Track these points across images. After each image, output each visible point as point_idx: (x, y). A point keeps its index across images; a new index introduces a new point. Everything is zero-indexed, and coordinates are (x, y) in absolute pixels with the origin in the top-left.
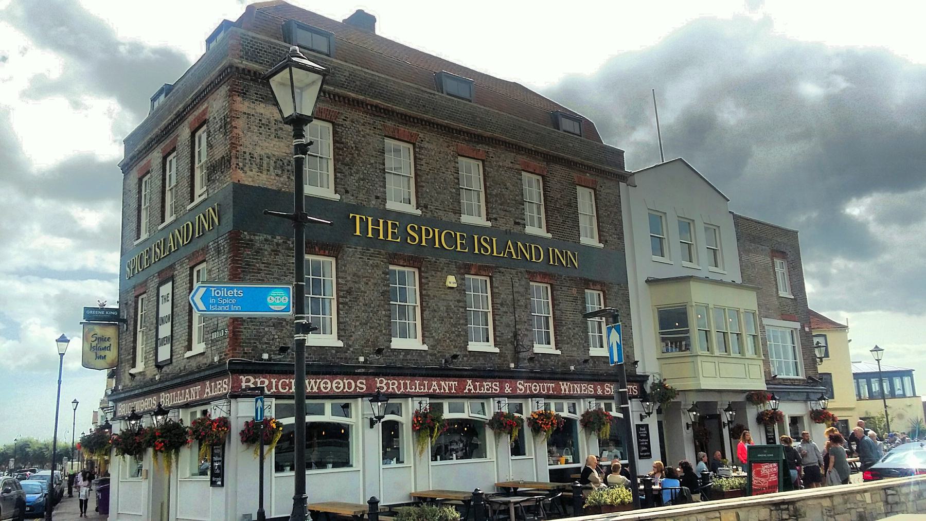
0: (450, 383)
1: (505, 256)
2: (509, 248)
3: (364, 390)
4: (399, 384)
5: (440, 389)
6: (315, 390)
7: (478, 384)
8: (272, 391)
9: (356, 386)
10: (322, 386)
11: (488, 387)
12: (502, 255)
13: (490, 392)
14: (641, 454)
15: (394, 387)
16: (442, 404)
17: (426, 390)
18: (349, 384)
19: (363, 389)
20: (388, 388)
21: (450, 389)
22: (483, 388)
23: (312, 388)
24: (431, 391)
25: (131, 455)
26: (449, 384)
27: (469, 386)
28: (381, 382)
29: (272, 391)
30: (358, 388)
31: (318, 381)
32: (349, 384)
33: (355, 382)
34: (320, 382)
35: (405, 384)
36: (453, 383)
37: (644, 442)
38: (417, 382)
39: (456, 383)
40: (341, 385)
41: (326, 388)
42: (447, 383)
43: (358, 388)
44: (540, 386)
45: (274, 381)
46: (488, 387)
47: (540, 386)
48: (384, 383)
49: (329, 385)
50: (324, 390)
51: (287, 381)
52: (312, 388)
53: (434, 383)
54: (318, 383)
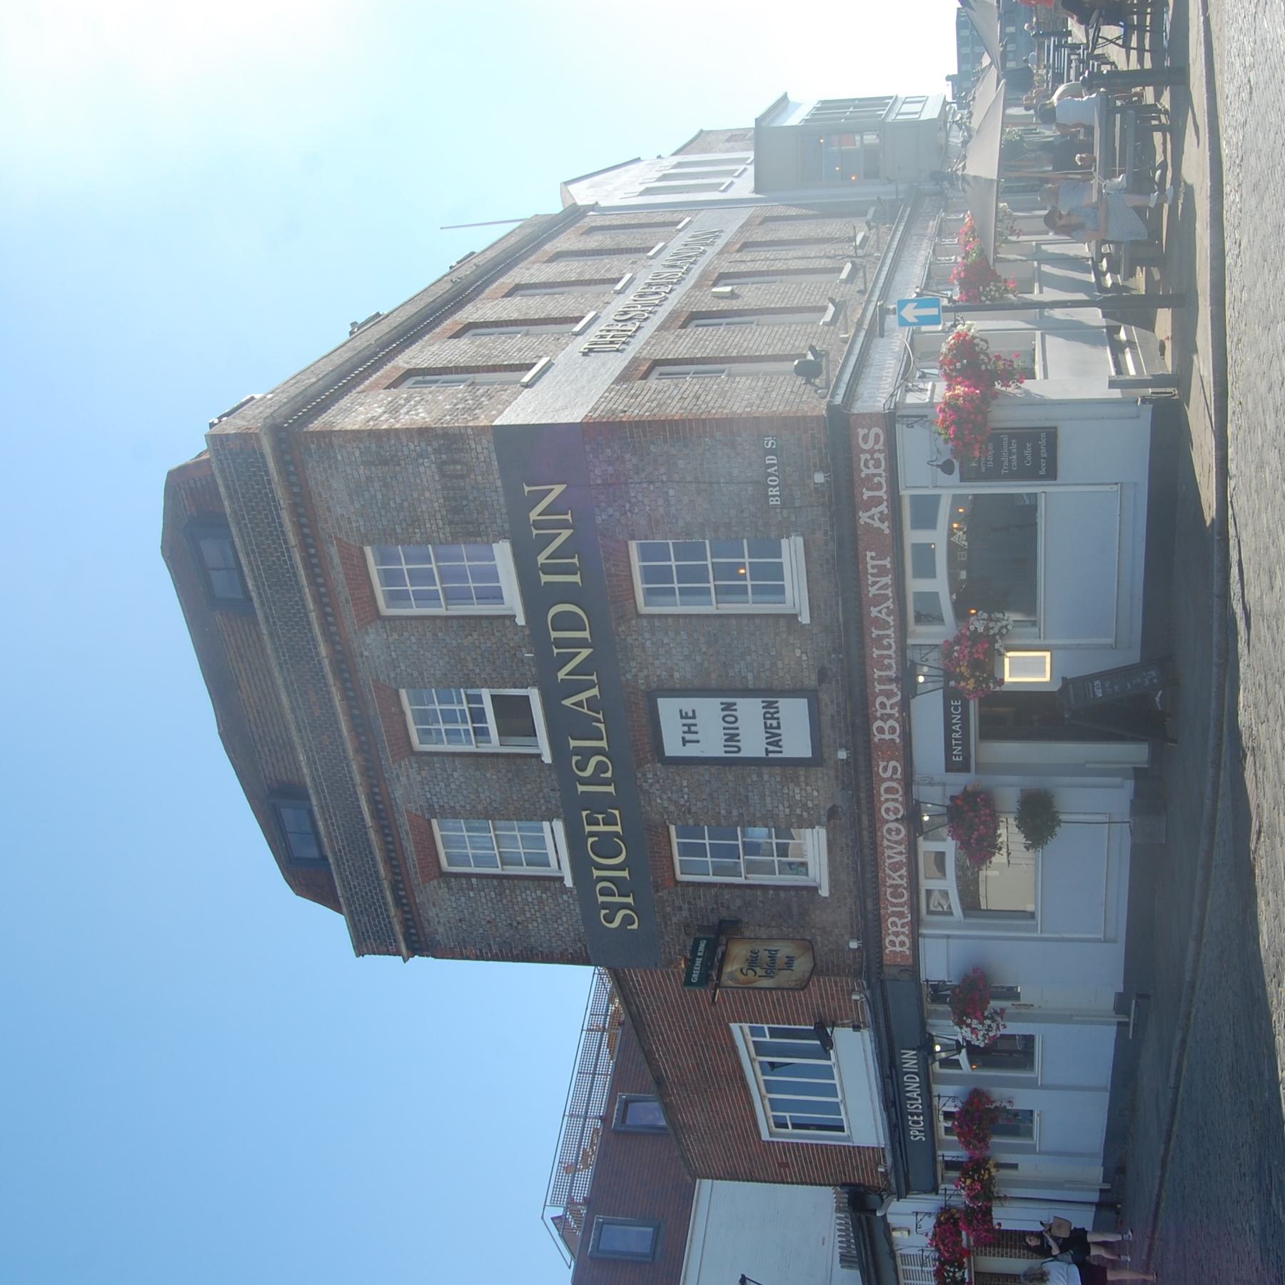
0: (871, 571)
1: (594, 677)
2: (579, 704)
3: (897, 764)
4: (894, 914)
5: (886, 597)
6: (902, 848)
7: (867, 494)
8: (895, 690)
9: (891, 779)
10: (894, 837)
11: (871, 463)
12: (602, 726)
13: (881, 456)
14: (1042, 472)
15: (899, 923)
16: (915, 546)
17: (890, 632)
18: (888, 790)
19: (877, 436)
20: (890, 716)
21: (882, 571)
22: (876, 480)
23: (900, 853)
24: (890, 619)
25: (994, 854)
26: (873, 575)
27: (872, 518)
28: (881, 730)
29: (895, 690)
30: (895, 777)
31: (886, 843)
32: (888, 790)
33: (887, 821)
34: (888, 840)
35: (882, 680)
36: (870, 563)
37: (1010, 453)
38: (876, 653)
39: (869, 554)
40: (890, 805)
41: (898, 831)
42: (871, 579)
43: (895, 777)
44: (887, 800)
45: (891, 909)
46: (871, 463)
47: (887, 800)
48: (894, 939)
49: (890, 805)
50: (902, 835)
51: (889, 891)
52: (900, 853)
53: (874, 612)
54: (889, 844)
